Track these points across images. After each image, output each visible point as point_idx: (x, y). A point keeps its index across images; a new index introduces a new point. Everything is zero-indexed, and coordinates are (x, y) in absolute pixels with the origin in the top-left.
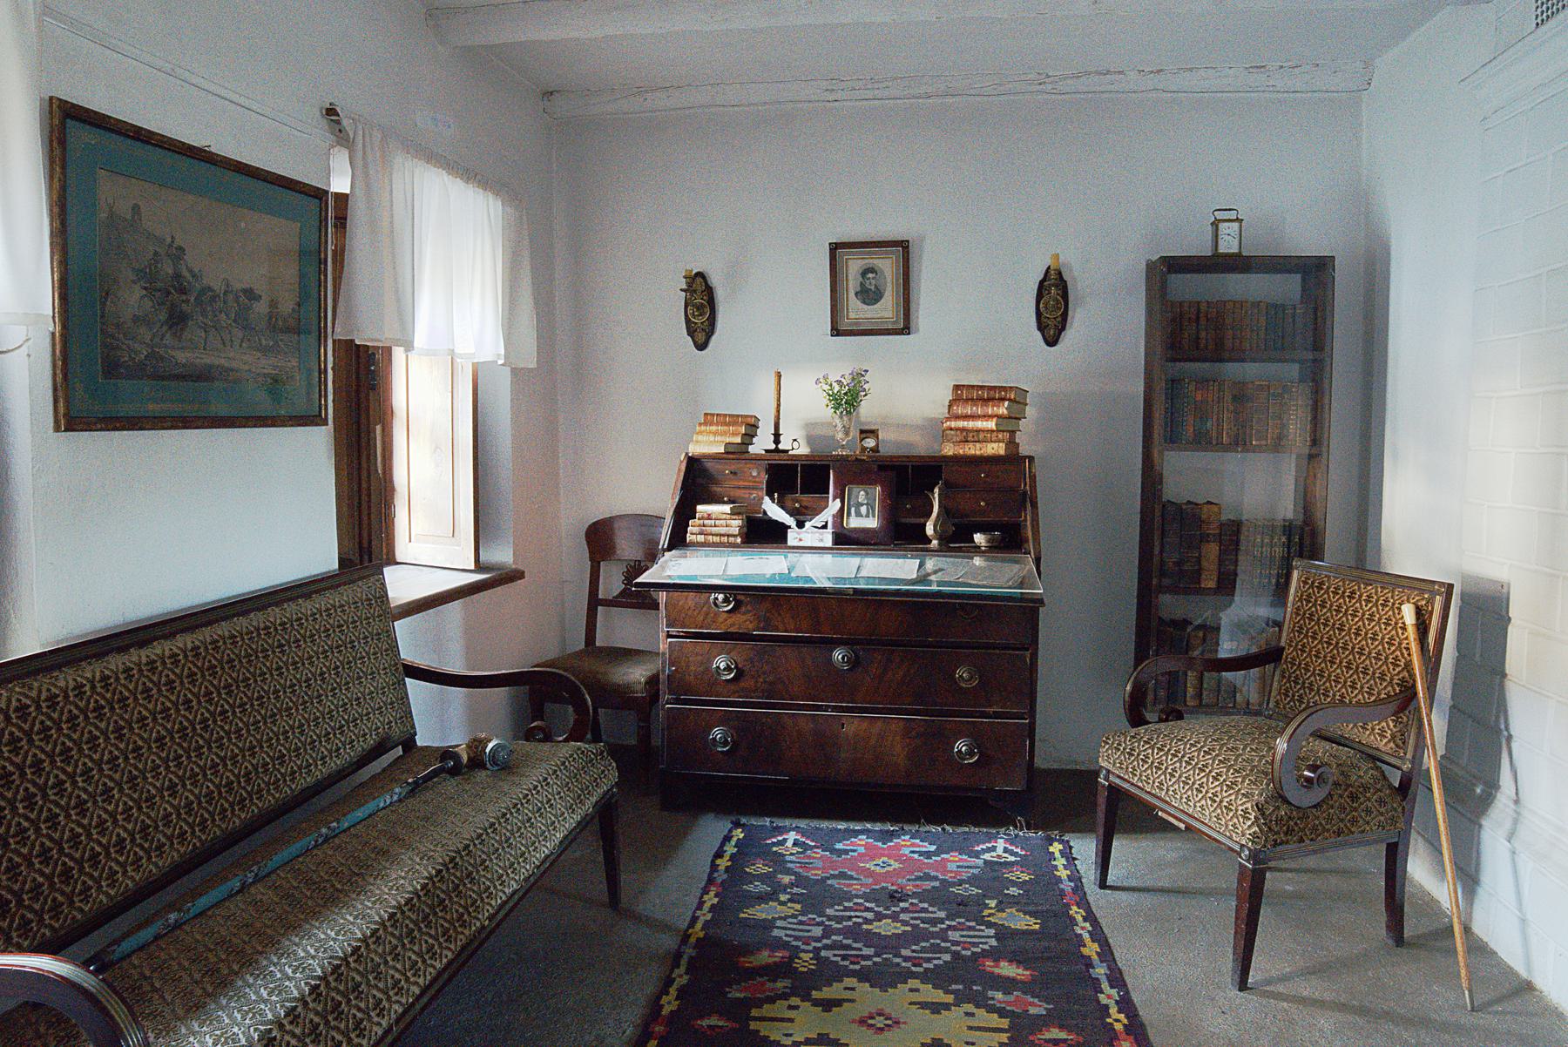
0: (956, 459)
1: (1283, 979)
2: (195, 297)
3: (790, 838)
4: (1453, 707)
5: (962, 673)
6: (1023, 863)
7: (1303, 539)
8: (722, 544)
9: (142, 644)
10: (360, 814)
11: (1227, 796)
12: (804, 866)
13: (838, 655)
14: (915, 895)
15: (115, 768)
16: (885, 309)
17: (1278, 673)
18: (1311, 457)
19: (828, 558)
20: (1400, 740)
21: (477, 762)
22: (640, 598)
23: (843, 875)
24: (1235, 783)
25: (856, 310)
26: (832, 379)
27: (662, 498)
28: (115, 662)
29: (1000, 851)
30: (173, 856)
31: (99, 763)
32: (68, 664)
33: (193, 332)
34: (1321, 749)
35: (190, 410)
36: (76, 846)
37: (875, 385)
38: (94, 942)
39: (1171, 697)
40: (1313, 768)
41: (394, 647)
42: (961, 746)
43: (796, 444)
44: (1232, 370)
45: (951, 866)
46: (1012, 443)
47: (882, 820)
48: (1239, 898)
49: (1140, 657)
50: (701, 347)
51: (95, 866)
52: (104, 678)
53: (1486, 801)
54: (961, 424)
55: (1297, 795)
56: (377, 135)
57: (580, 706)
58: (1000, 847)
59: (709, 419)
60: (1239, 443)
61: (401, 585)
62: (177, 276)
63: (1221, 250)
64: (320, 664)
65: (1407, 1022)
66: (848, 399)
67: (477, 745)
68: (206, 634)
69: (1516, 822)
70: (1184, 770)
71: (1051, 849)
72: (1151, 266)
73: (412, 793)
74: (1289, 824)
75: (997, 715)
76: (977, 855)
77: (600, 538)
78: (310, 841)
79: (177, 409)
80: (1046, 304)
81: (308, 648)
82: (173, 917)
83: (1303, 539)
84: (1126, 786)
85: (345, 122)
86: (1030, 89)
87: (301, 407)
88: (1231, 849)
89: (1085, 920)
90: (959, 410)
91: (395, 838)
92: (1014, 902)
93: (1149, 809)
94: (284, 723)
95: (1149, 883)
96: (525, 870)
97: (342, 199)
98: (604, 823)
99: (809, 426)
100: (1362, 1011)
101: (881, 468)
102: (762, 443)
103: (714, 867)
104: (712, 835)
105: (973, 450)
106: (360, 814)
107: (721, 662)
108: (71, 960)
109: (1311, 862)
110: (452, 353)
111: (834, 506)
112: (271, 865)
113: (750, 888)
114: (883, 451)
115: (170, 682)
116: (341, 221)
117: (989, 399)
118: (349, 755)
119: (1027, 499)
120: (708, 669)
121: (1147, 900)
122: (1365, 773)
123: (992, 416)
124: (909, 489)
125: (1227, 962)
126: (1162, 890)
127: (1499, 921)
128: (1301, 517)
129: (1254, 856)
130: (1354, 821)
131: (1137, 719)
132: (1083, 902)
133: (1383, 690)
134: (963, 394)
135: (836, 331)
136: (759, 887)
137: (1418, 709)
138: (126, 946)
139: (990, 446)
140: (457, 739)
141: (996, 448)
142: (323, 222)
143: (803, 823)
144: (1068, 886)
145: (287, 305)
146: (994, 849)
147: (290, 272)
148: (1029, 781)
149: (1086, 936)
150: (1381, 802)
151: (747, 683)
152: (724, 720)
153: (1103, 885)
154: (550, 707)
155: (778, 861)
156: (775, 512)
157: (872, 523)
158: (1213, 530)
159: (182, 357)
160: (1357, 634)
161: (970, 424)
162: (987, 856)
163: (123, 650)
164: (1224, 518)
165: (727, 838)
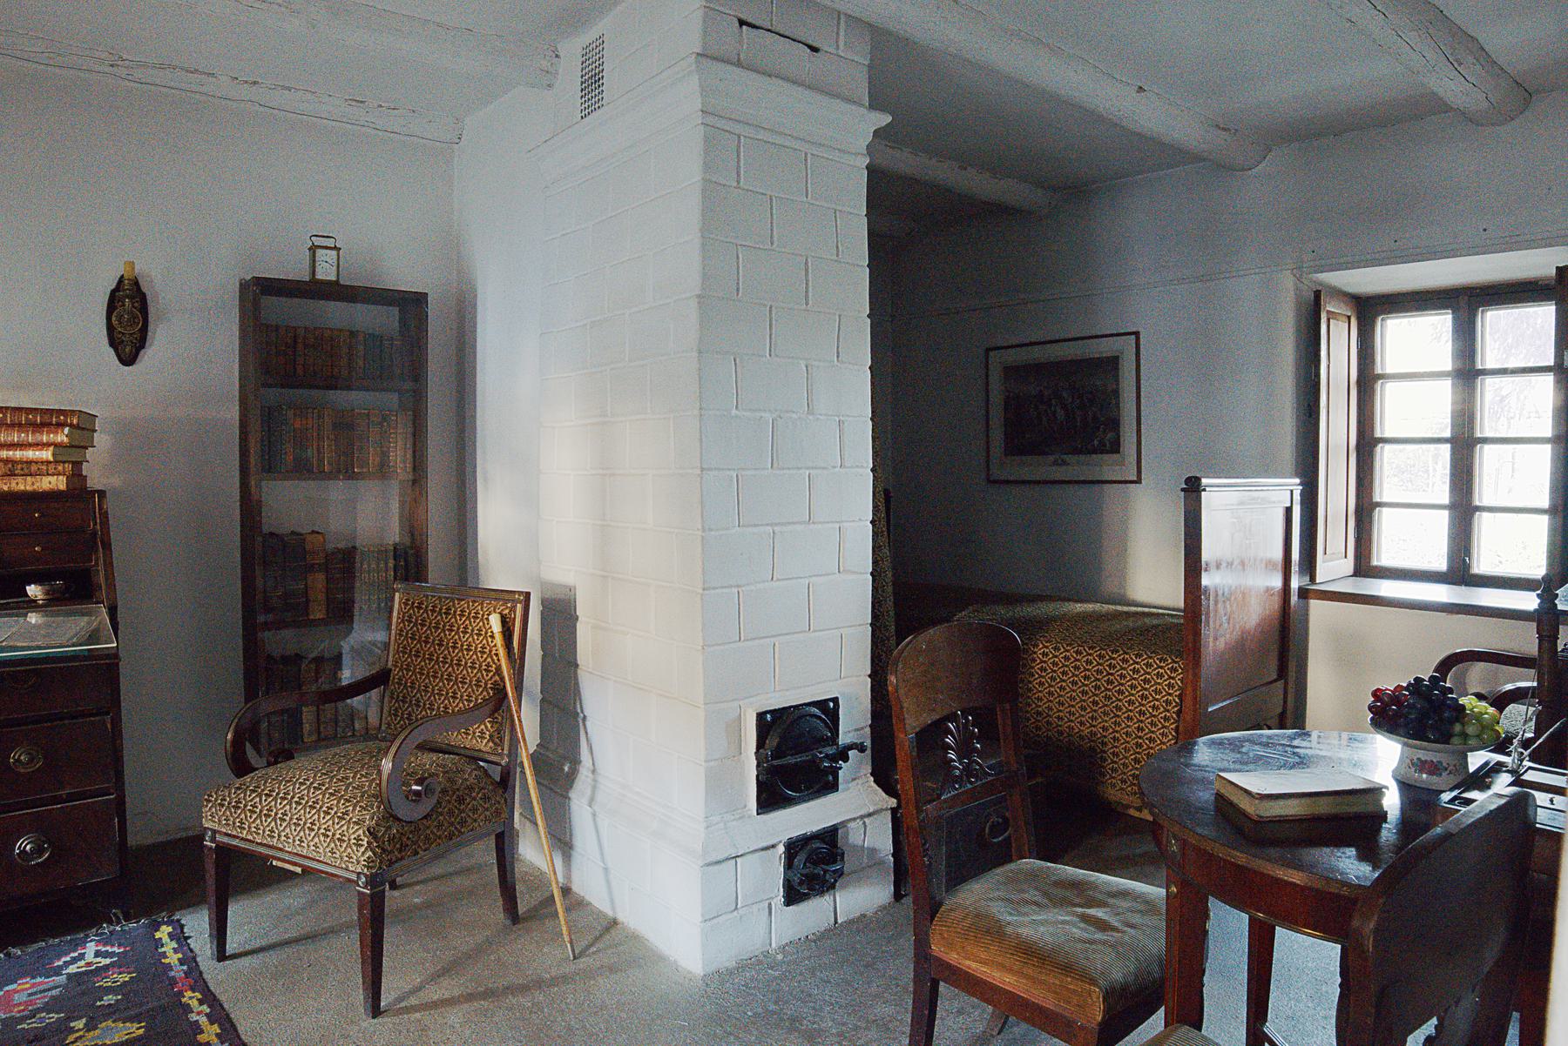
1: (416, 990)
4: (542, 701)
5: (19, 756)
6: (121, 964)
7: (409, 562)
11: (338, 829)
17: (388, 693)
18: (414, 482)
20: (497, 739)
24: (346, 813)
29: (90, 957)
34: (428, 759)
42: (24, 844)
44: (340, 398)
48: (362, 929)
53: (571, 778)
55: (405, 811)
60: (347, 470)
63: (319, 276)
65: (523, 989)
69: (594, 788)
71: (158, 935)
72: (244, 286)
74: (402, 842)
76: (57, 972)
80: (120, 317)
83: (409, 562)
84: (235, 842)
86: (97, 68)
88: (349, 880)
89: (201, 1002)
92: (111, 1012)
95: (274, 939)
100: (489, 994)
105: (21, 485)
109: (437, 869)
117: (43, 425)
121: (272, 958)
122: (469, 775)
123: (48, 445)
125: (359, 996)
126: (287, 943)
127: (589, 882)
128: (407, 541)
129: (372, 881)
131: (241, 767)
132: (196, 978)
133: (480, 695)
137: (509, 707)
139: (46, 479)
141: (55, 483)
144: (178, 971)
146: (82, 957)
149: (203, 1020)
150: (486, 798)
158: (320, 560)
160: (454, 647)
161: (18, 454)
162: (72, 969)
164: (330, 546)
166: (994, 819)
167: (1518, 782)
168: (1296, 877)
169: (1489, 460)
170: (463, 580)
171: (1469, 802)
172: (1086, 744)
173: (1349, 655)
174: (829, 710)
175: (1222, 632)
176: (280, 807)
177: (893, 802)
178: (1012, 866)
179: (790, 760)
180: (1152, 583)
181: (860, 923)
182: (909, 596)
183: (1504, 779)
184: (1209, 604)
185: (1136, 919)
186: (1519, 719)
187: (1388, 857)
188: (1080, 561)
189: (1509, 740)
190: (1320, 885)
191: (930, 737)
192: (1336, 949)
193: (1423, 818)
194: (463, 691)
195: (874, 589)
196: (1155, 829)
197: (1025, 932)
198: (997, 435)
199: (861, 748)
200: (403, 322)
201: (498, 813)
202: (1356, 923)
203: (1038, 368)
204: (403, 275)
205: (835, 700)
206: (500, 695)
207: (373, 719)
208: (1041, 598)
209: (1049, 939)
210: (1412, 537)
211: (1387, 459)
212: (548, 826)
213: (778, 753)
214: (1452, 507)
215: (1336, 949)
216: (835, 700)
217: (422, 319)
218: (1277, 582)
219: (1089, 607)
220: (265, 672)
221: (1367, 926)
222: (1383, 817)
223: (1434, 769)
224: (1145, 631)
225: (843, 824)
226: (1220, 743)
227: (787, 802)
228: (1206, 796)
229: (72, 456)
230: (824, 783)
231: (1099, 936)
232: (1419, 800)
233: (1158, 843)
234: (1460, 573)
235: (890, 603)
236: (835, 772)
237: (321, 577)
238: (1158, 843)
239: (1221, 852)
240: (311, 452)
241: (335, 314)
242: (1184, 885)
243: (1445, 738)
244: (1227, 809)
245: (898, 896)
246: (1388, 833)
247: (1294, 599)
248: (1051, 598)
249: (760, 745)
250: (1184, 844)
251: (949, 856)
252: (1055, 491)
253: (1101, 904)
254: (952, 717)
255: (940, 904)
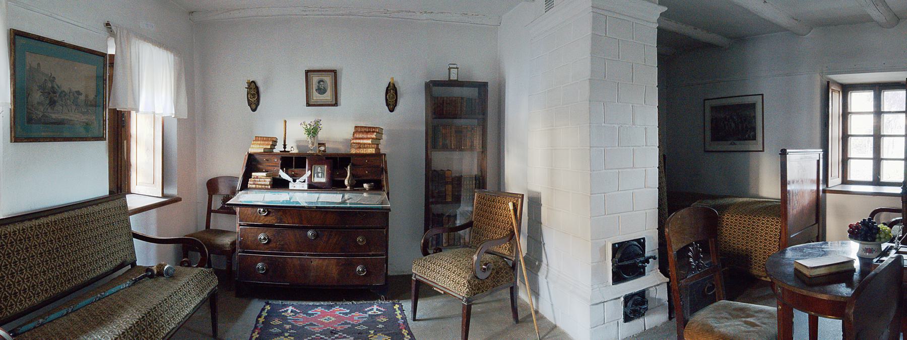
0: (356, 155)
2: (65, 95)
3: (290, 309)
5: (359, 239)
6: (384, 314)
7: (480, 182)
8: (263, 189)
9: (37, 218)
10: (113, 290)
11: (458, 279)
12: (295, 321)
13: (310, 233)
14: (341, 331)
15: (25, 262)
16: (328, 96)
19: (306, 194)
21: (160, 274)
22: (229, 210)
23: (311, 324)
25: (316, 97)
26: (307, 123)
27: (238, 170)
28: (27, 224)
30: (43, 297)
31: (19, 260)
32: (11, 223)
33: (58, 107)
34: (488, 257)
35: (57, 135)
36: (10, 288)
37: (324, 125)
38: (13, 325)
39: (437, 243)
40: (486, 265)
41: (129, 226)
42: (359, 268)
43: (292, 149)
45: (356, 318)
46: (377, 149)
47: (328, 300)
49: (426, 229)
50: (254, 110)
51: (15, 297)
52: (23, 229)
53: (538, 268)
54: (358, 141)
56: (125, 32)
57: (203, 253)
58: (375, 308)
59: (257, 138)
60: (459, 148)
61: (133, 202)
62: (53, 87)
64: (101, 231)
66: (313, 131)
67: (161, 266)
68: (59, 216)
70: (443, 271)
73: (134, 284)
74: (479, 286)
75: (373, 255)
77: (212, 186)
78: (93, 299)
79: (51, 134)
81: (96, 224)
82: (41, 320)
85: (113, 28)
87: (96, 134)
90: (357, 136)
91: (126, 302)
92: (381, 330)
93: (431, 287)
94: (86, 252)
95: (431, 317)
96: (178, 319)
97: (112, 56)
98: (212, 301)
99: (298, 141)
101: (327, 158)
102: (279, 148)
103: (257, 321)
104: (256, 308)
105: (363, 151)
106: (113, 290)
107: (262, 236)
108: (4, 330)
109: (486, 299)
110: (154, 113)
111: (308, 173)
112: (78, 306)
113: (272, 330)
114: (328, 152)
115: (46, 233)
116: (112, 65)
118: (110, 267)
119: (384, 170)
120: (256, 239)
121: (430, 323)
122: (501, 264)
124: (339, 167)
127: (545, 310)
129: (468, 300)
130: (498, 281)
131: (425, 253)
132: (407, 328)
133: (505, 233)
134: (358, 130)
135: (308, 105)
136: (276, 330)
138: (24, 328)
140: (153, 264)
141: (372, 151)
142: (105, 65)
143: (295, 303)
144: (401, 322)
145: (92, 97)
147: (93, 84)
148: (386, 280)
150: (507, 273)
151: (272, 245)
152: (263, 260)
153: (414, 319)
154: (190, 253)
155: (284, 319)
156: (284, 175)
157: (323, 180)
159: (54, 116)
161: (361, 141)
163: (30, 220)
165: (263, 309)
166: (709, 285)
167: (898, 252)
168: (824, 297)
169: (885, 142)
170: (499, 189)
171: (882, 261)
172: (744, 253)
173: (841, 212)
174: (641, 242)
175: (795, 208)
176: (438, 268)
177: (668, 280)
178: (716, 304)
179: (626, 263)
180: (769, 189)
181: (655, 330)
182: (673, 196)
183: (894, 251)
184: (790, 196)
185: (766, 321)
186: (897, 230)
187: (856, 285)
188: (740, 182)
189: (894, 238)
190: (833, 299)
191: (682, 253)
192: (839, 322)
193: (868, 269)
194: (499, 231)
195: (659, 194)
196: (772, 285)
197: (722, 330)
198: (708, 133)
199: (654, 258)
200: (479, 93)
201: (511, 279)
202: (847, 311)
203: (725, 108)
204: (479, 76)
205: (644, 239)
206: (512, 234)
207: (467, 240)
208: (726, 197)
209: (732, 332)
210: (861, 170)
211: (852, 141)
212: (530, 286)
213: (621, 260)
214: (874, 159)
215: (839, 322)
216: (644, 239)
217: (486, 92)
218: (815, 188)
219: (745, 199)
220: (432, 220)
221: (850, 311)
222: (854, 270)
223: (870, 251)
224: (766, 208)
225: (647, 289)
226: (795, 249)
227: (623, 280)
228: (790, 270)
229: (376, 142)
230: (638, 272)
231: (752, 329)
232: (866, 263)
233: (773, 289)
234: (877, 182)
235: (665, 200)
236: (644, 268)
237: (450, 186)
238: (773, 289)
239: (797, 291)
240: (448, 142)
241: (457, 92)
242: (784, 305)
243: (874, 240)
244: (799, 274)
245: (670, 318)
246: (856, 276)
247: (821, 193)
248: (730, 197)
249: (613, 257)
250: (783, 289)
251: (691, 301)
252: (731, 155)
253: (752, 316)
254: (691, 245)
255: (688, 321)
